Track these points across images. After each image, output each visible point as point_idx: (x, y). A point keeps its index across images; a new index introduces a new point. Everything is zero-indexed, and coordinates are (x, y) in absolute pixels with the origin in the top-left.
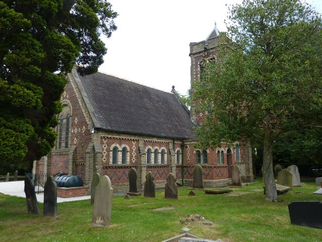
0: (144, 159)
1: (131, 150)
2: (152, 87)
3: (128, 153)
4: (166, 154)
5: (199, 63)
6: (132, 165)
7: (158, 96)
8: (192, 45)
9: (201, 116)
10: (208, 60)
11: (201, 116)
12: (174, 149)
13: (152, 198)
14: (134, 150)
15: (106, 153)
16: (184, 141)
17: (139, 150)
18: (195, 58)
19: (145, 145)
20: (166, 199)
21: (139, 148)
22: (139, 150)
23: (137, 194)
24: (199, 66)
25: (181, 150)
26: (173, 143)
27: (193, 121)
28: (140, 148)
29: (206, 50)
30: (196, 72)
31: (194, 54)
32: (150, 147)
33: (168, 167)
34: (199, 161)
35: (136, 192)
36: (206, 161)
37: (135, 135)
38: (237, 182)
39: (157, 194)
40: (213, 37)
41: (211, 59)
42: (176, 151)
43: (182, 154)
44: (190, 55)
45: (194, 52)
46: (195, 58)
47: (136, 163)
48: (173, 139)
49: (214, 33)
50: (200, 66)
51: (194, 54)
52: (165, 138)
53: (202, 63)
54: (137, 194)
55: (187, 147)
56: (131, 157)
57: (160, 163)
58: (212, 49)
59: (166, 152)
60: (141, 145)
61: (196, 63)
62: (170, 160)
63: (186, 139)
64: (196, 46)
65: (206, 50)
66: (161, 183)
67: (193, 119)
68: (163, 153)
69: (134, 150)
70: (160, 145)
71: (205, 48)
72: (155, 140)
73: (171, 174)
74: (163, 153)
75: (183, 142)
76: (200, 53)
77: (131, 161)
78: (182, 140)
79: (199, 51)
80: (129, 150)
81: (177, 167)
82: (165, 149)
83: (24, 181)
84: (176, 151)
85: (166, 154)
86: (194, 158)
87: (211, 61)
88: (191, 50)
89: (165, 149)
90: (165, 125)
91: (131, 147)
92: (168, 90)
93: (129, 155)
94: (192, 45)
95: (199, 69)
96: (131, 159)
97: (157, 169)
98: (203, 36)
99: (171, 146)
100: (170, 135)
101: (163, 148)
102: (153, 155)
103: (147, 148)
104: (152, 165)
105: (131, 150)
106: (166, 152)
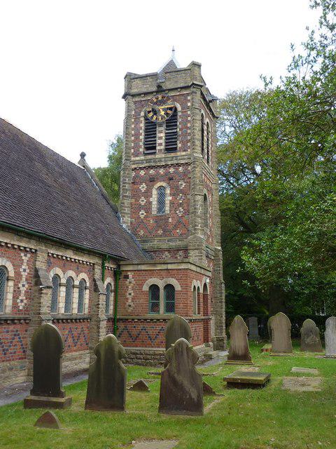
0: (46, 299)
1: (18, 274)
2: (45, 144)
3: (11, 283)
4: (87, 291)
5: (142, 114)
6: (17, 316)
7: (57, 164)
8: (130, 78)
9: (142, 217)
10: (163, 110)
11: (142, 217)
12: (103, 280)
13: (110, 415)
14: (24, 274)
15: (21, 270)
16: (122, 263)
17: (36, 277)
18: (135, 103)
19: (50, 266)
20: (165, 417)
21: (36, 271)
22: (36, 277)
23: (62, 400)
24: (142, 119)
25: (113, 284)
26: (103, 264)
27: (124, 226)
28: (40, 273)
29: (160, 89)
30: (137, 129)
31: (133, 96)
32: (58, 271)
33: (89, 320)
34: (155, 307)
35: (61, 395)
36: (170, 308)
37: (30, 236)
38: (241, 353)
39: (131, 396)
40: (171, 69)
41: (171, 109)
42: (106, 283)
43: (115, 291)
44: (124, 97)
45: (134, 91)
46: (135, 103)
47: (27, 309)
48: (103, 257)
49: (171, 64)
50: (146, 119)
51: (133, 96)
52: (90, 252)
53: (151, 114)
54: (62, 400)
55: (127, 277)
56: (17, 293)
57: (62, 311)
58: (170, 90)
59: (88, 284)
60: (41, 264)
61: (137, 117)
62: (95, 305)
63: (124, 259)
64: (138, 81)
65: (160, 89)
66: (75, 359)
67: (124, 222)
68: (82, 287)
69: (24, 274)
70: (78, 266)
71: (159, 87)
72: (69, 254)
73: (181, 344)
74: (82, 287)
75: (119, 266)
76: (146, 94)
77: (15, 305)
78: (117, 260)
79: (145, 90)
80: (12, 274)
81: (109, 320)
82: (87, 280)
83: (99, 160)
84: (106, 283)
85: (87, 291)
86: (145, 301)
87: (169, 112)
88: (129, 86)
89: (87, 280)
90: (83, 225)
91: (16, 267)
92: (75, 159)
93: (11, 289)
94: (130, 78)
95: (142, 125)
96: (15, 297)
97: (70, 325)
98: (152, 64)
99: (98, 270)
100: (98, 248)
101: (83, 276)
102: (63, 291)
103: (52, 274)
104: (74, 317)
105: (18, 274)
106: (88, 284)
